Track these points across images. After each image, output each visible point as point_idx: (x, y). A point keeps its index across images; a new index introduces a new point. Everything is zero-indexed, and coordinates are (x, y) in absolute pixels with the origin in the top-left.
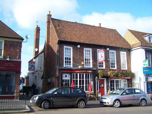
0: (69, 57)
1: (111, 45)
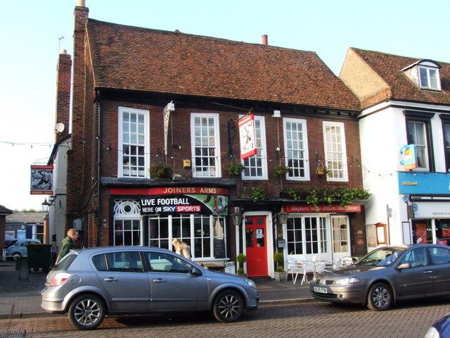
0: (137, 144)
1: (287, 99)
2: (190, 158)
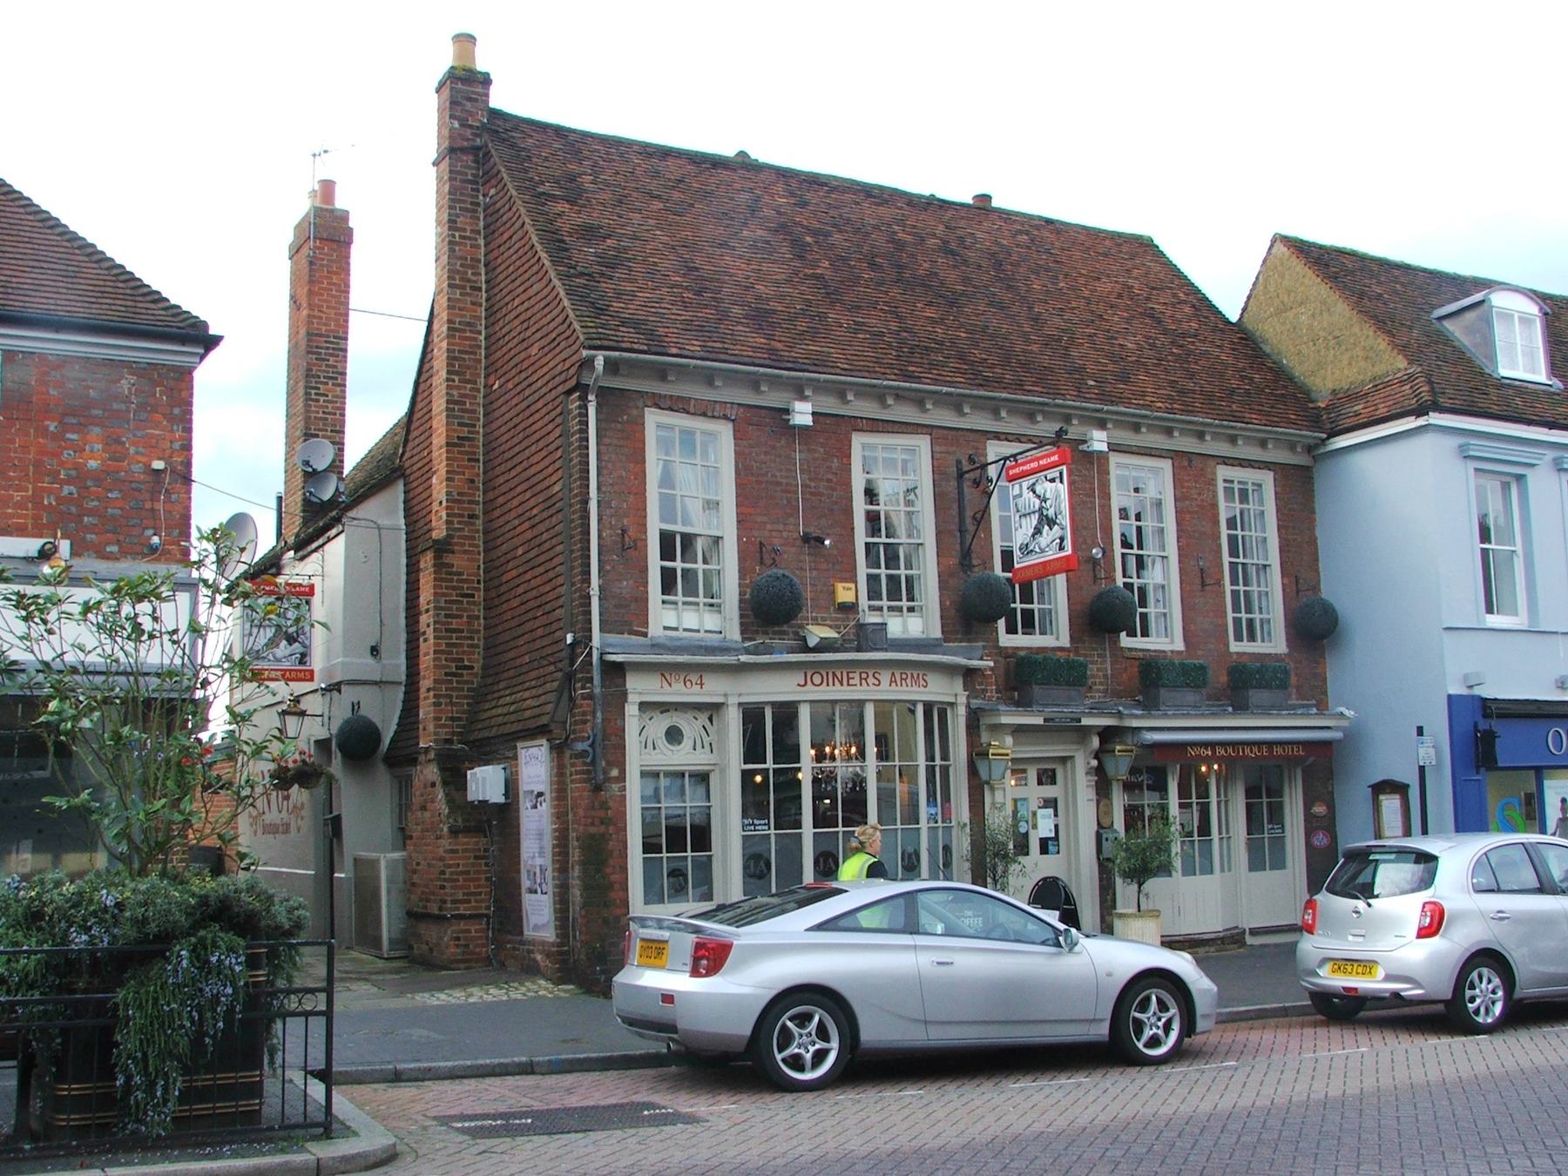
2: (854, 579)
